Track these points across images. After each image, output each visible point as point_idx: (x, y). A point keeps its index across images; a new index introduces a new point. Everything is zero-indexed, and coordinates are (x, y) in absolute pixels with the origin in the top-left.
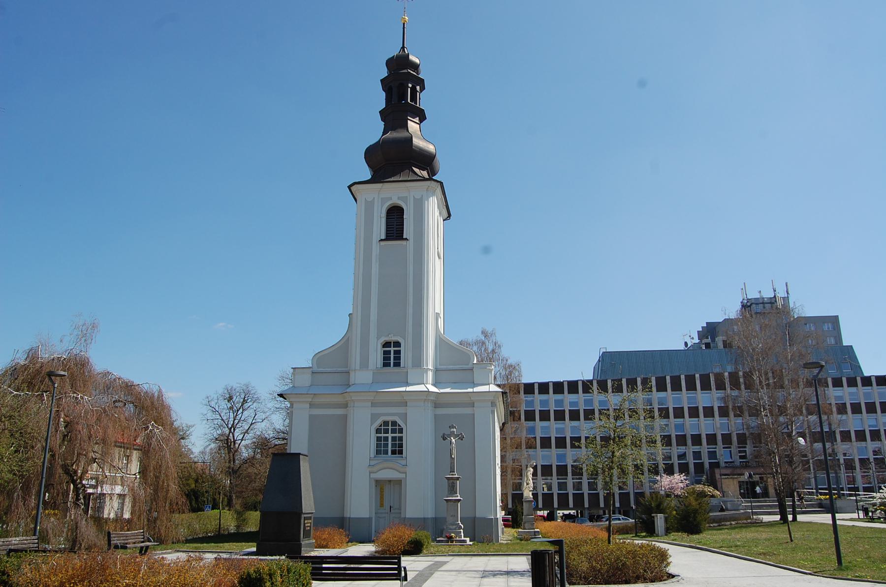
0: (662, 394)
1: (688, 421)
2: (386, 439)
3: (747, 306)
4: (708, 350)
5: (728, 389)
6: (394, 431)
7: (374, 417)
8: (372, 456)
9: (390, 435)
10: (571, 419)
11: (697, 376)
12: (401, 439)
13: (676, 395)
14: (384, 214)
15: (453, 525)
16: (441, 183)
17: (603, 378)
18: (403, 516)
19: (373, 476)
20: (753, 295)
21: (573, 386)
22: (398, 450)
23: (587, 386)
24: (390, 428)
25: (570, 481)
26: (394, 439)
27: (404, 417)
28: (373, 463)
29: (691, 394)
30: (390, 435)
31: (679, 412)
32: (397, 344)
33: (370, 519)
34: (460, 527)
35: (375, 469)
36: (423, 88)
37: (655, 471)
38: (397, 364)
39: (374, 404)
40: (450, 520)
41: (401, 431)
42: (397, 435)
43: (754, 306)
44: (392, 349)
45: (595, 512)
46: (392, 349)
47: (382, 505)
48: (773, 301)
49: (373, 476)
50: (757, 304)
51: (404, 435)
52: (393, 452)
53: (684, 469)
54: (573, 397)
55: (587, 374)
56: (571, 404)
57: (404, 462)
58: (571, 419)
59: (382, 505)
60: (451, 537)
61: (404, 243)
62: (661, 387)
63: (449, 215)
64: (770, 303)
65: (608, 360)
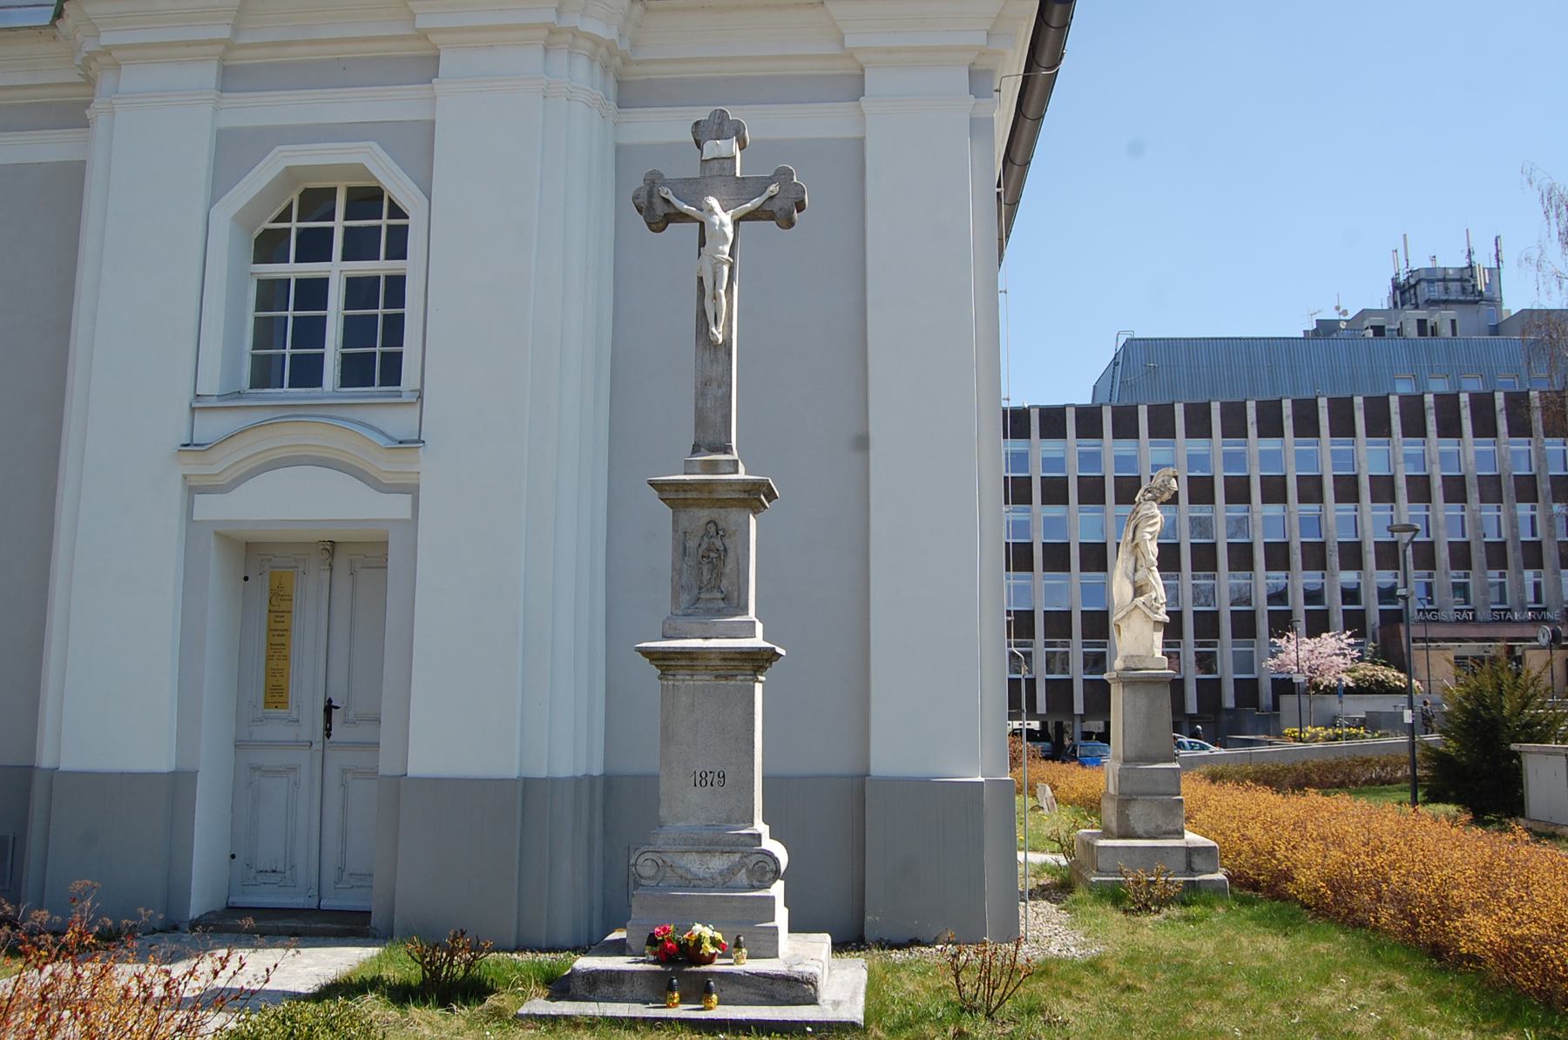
0: (1271, 444)
1: (1333, 511)
2: (313, 292)
3: (1404, 291)
4: (1380, 341)
6: (359, 245)
7: (232, 152)
8: (211, 384)
9: (337, 271)
10: (1046, 500)
11: (1358, 401)
12: (397, 285)
13: (1307, 445)
15: (708, 847)
17: (1126, 402)
18: (387, 766)
19: (211, 509)
20: (1420, 262)
21: (1053, 421)
23: (1089, 421)
24: (339, 225)
25: (1077, 648)
26: (359, 291)
27: (418, 142)
29: (1343, 445)
31: (1311, 489)
33: (175, 788)
34: (766, 870)
35: (218, 465)
37: (1281, 624)
39: (231, 77)
40: (686, 806)
42: (380, 267)
43: (1424, 285)
47: (276, 694)
48: (1466, 276)
49: (211, 509)
50: (1431, 282)
51: (410, 267)
52: (356, 372)
53: (1355, 622)
54: (1052, 447)
55: (1080, 394)
56: (1047, 463)
57: (399, 421)
58: (1046, 500)
59: (276, 694)
60: (691, 953)
62: (1270, 426)
64: (1461, 280)
65: (1138, 357)
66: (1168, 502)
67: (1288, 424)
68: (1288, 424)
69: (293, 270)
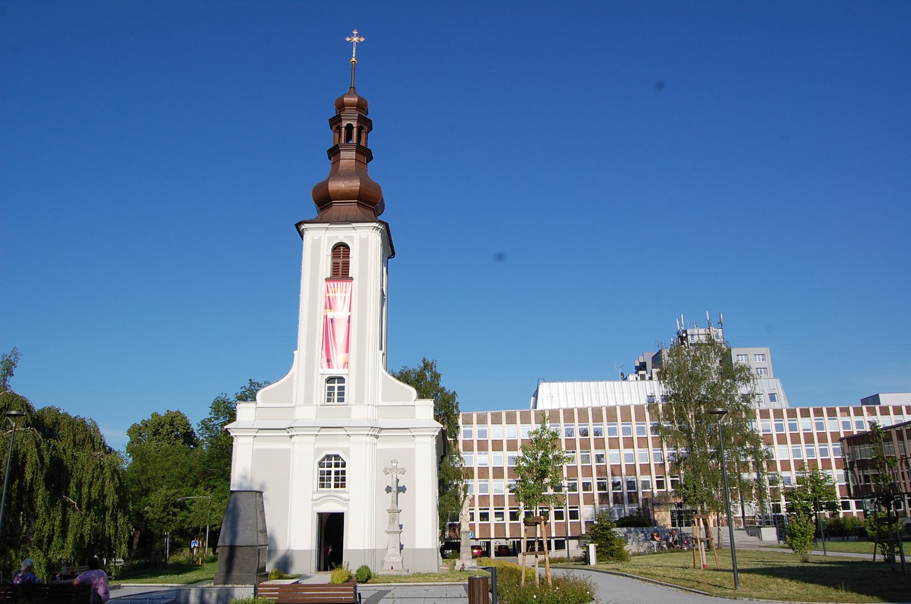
2: (329, 473)
5: (611, 504)
6: (337, 465)
7: (317, 451)
12: (344, 472)
14: (330, 252)
16: (386, 225)
22: (341, 482)
26: (337, 473)
28: (316, 496)
30: (333, 469)
32: (341, 379)
36: (370, 129)
38: (341, 400)
41: (344, 465)
42: (340, 469)
44: (336, 385)
45: (529, 492)
46: (336, 385)
52: (336, 486)
57: (345, 496)
61: (349, 284)
63: (394, 254)
66: (680, 462)
67: (475, 420)
68: (475, 420)
69: (326, 469)
